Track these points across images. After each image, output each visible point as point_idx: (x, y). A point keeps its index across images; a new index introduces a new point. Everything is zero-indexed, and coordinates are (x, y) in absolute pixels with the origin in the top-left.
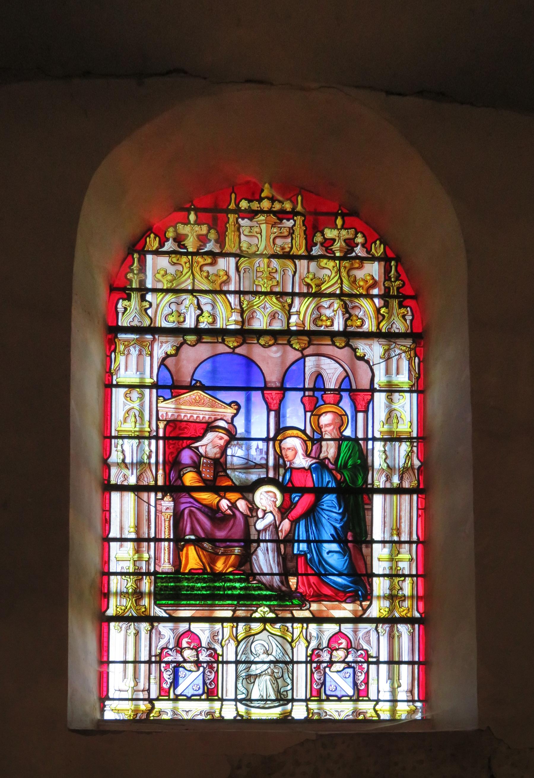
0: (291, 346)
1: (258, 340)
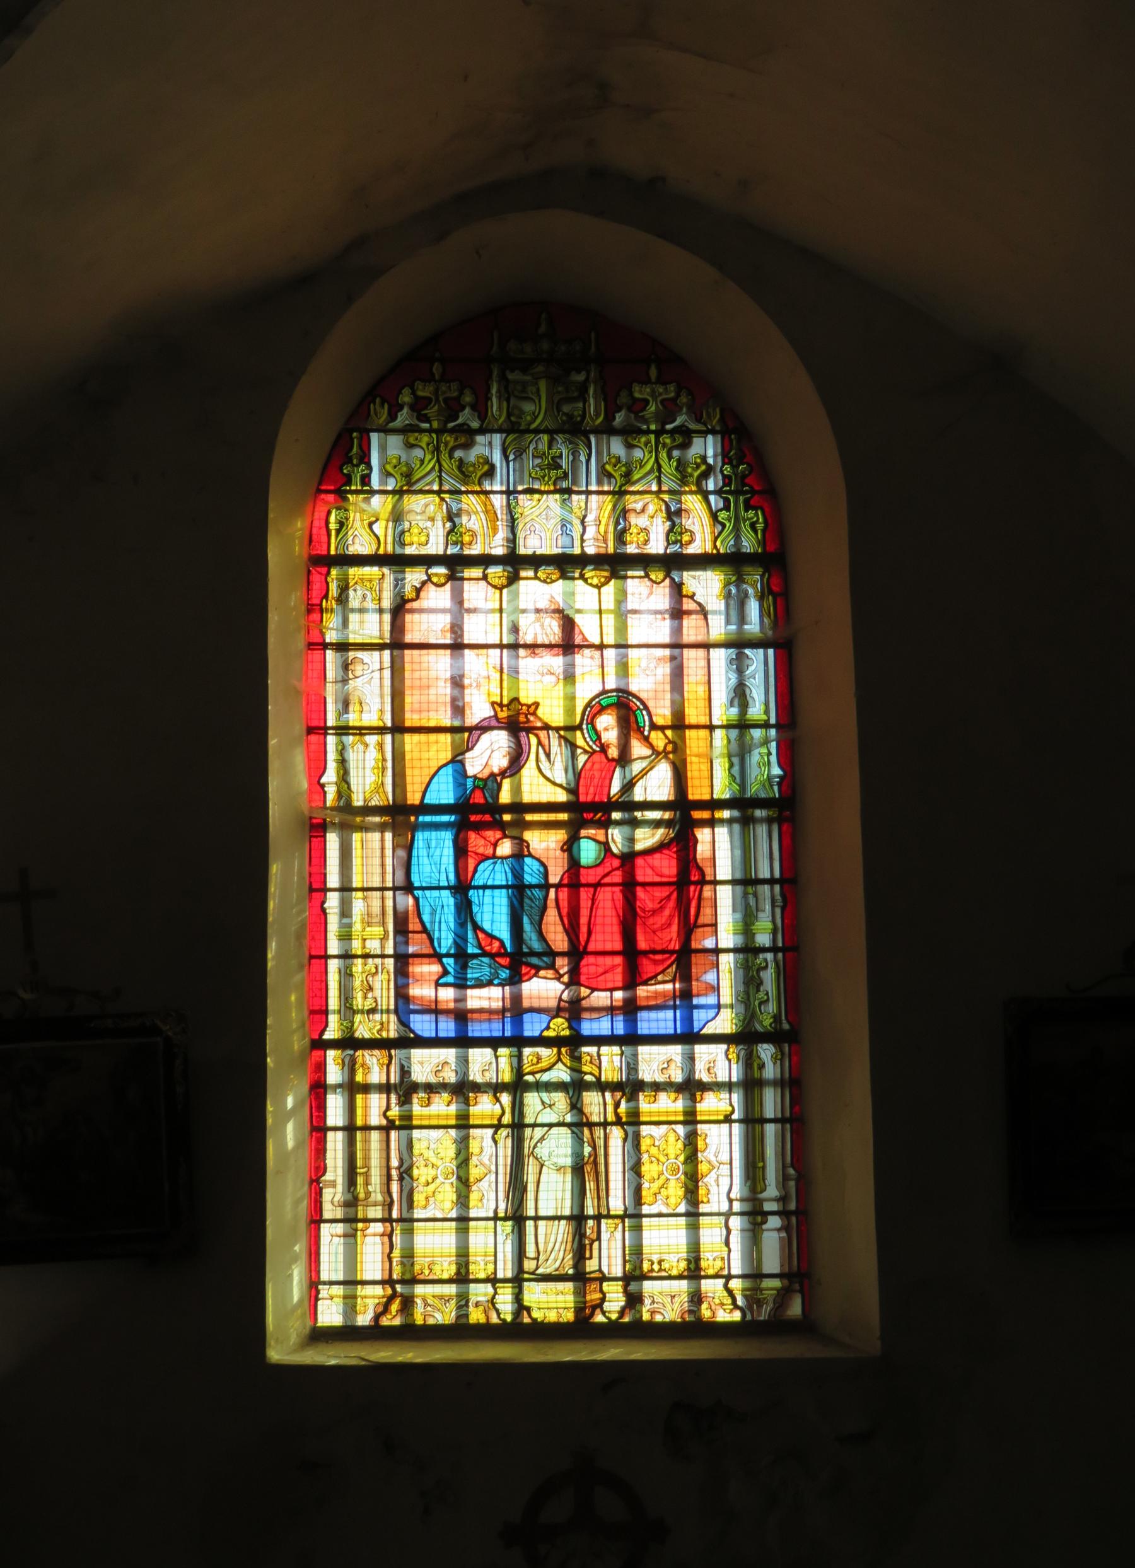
0: (586, 580)
1: (536, 572)
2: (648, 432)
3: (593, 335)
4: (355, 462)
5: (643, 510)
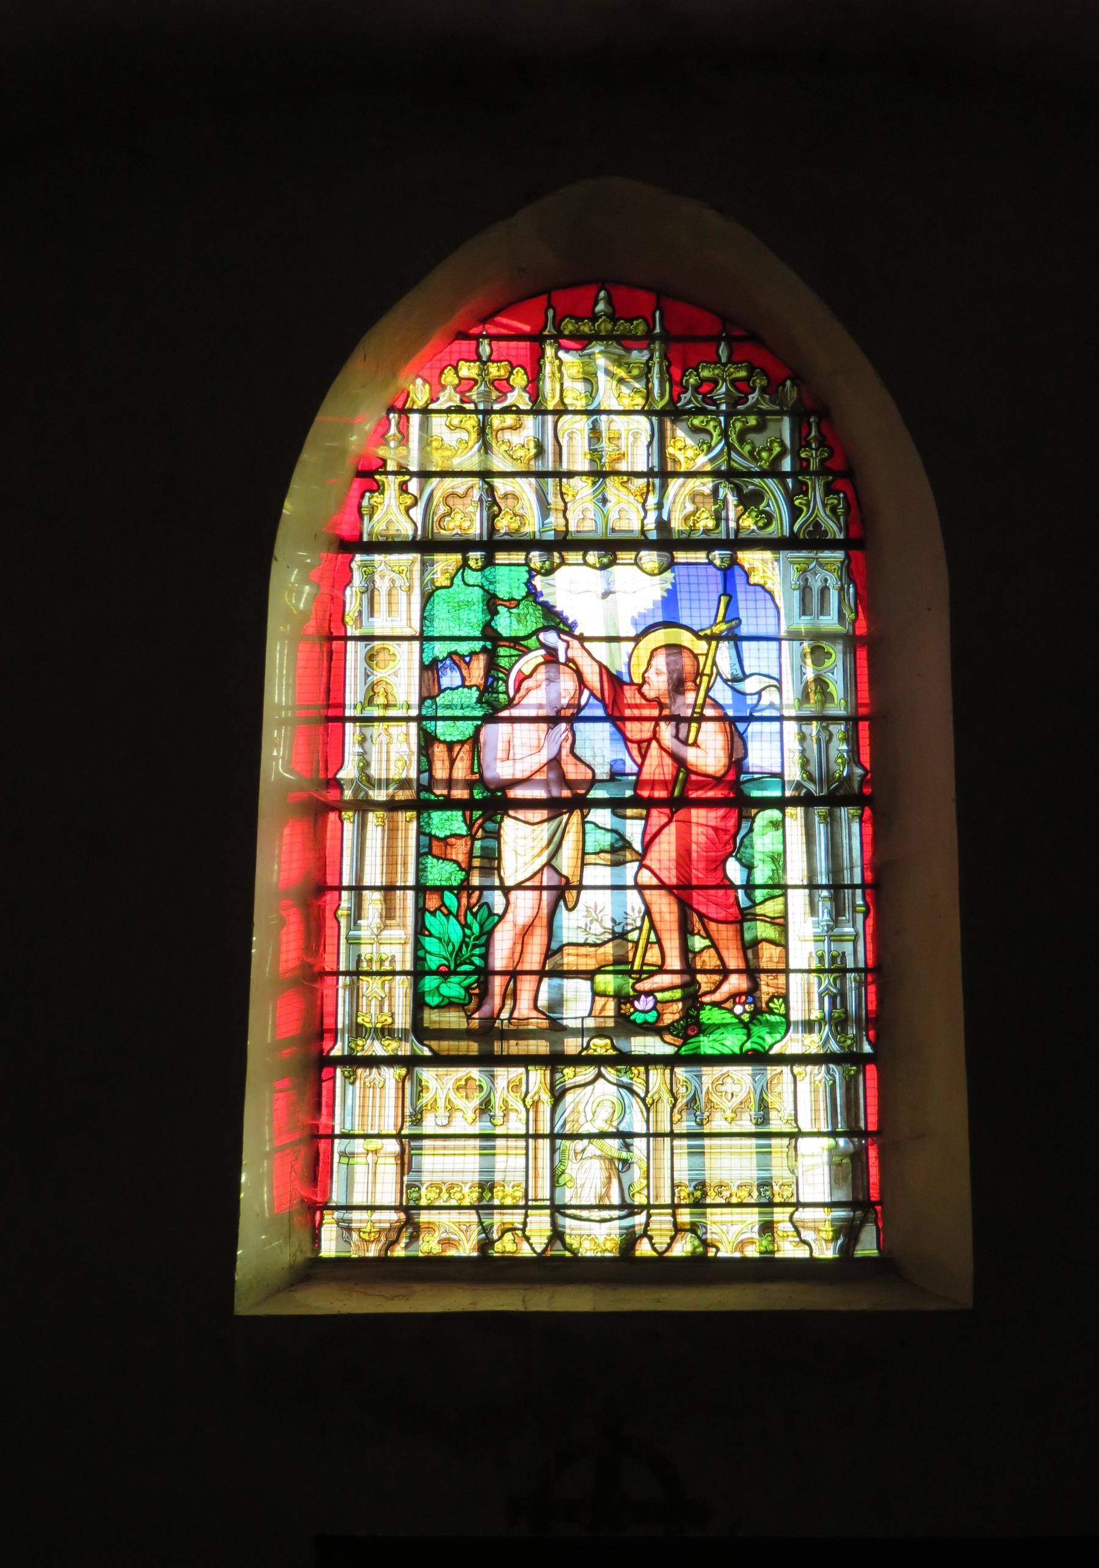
2: (717, 413)
3: (658, 314)
4: (814, 446)
5: (465, 495)
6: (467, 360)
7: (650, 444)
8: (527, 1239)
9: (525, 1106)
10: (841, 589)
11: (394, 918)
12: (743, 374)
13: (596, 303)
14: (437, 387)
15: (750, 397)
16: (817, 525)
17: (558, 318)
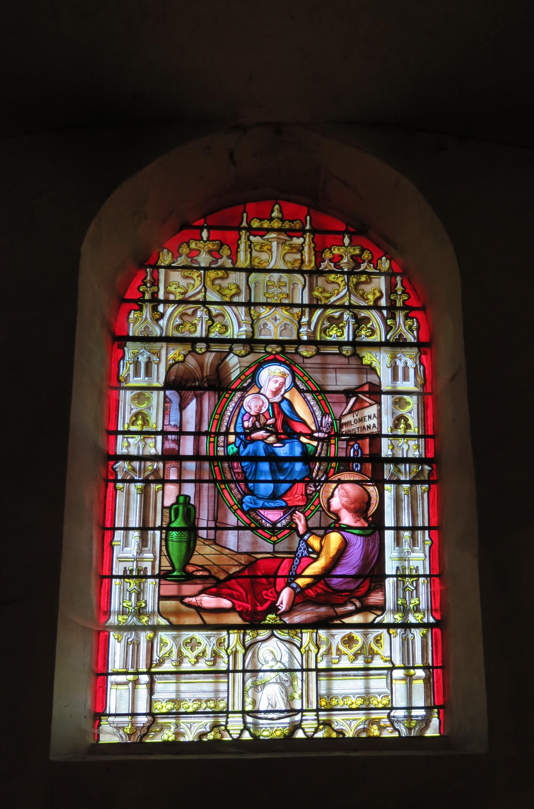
3: (308, 218)
4: (148, 285)
6: (195, 240)
7: (304, 286)
8: (228, 731)
9: (227, 654)
10: (416, 369)
11: (146, 546)
12: (357, 252)
13: (273, 211)
14: (176, 255)
15: (362, 265)
16: (401, 335)
17: (249, 219)
